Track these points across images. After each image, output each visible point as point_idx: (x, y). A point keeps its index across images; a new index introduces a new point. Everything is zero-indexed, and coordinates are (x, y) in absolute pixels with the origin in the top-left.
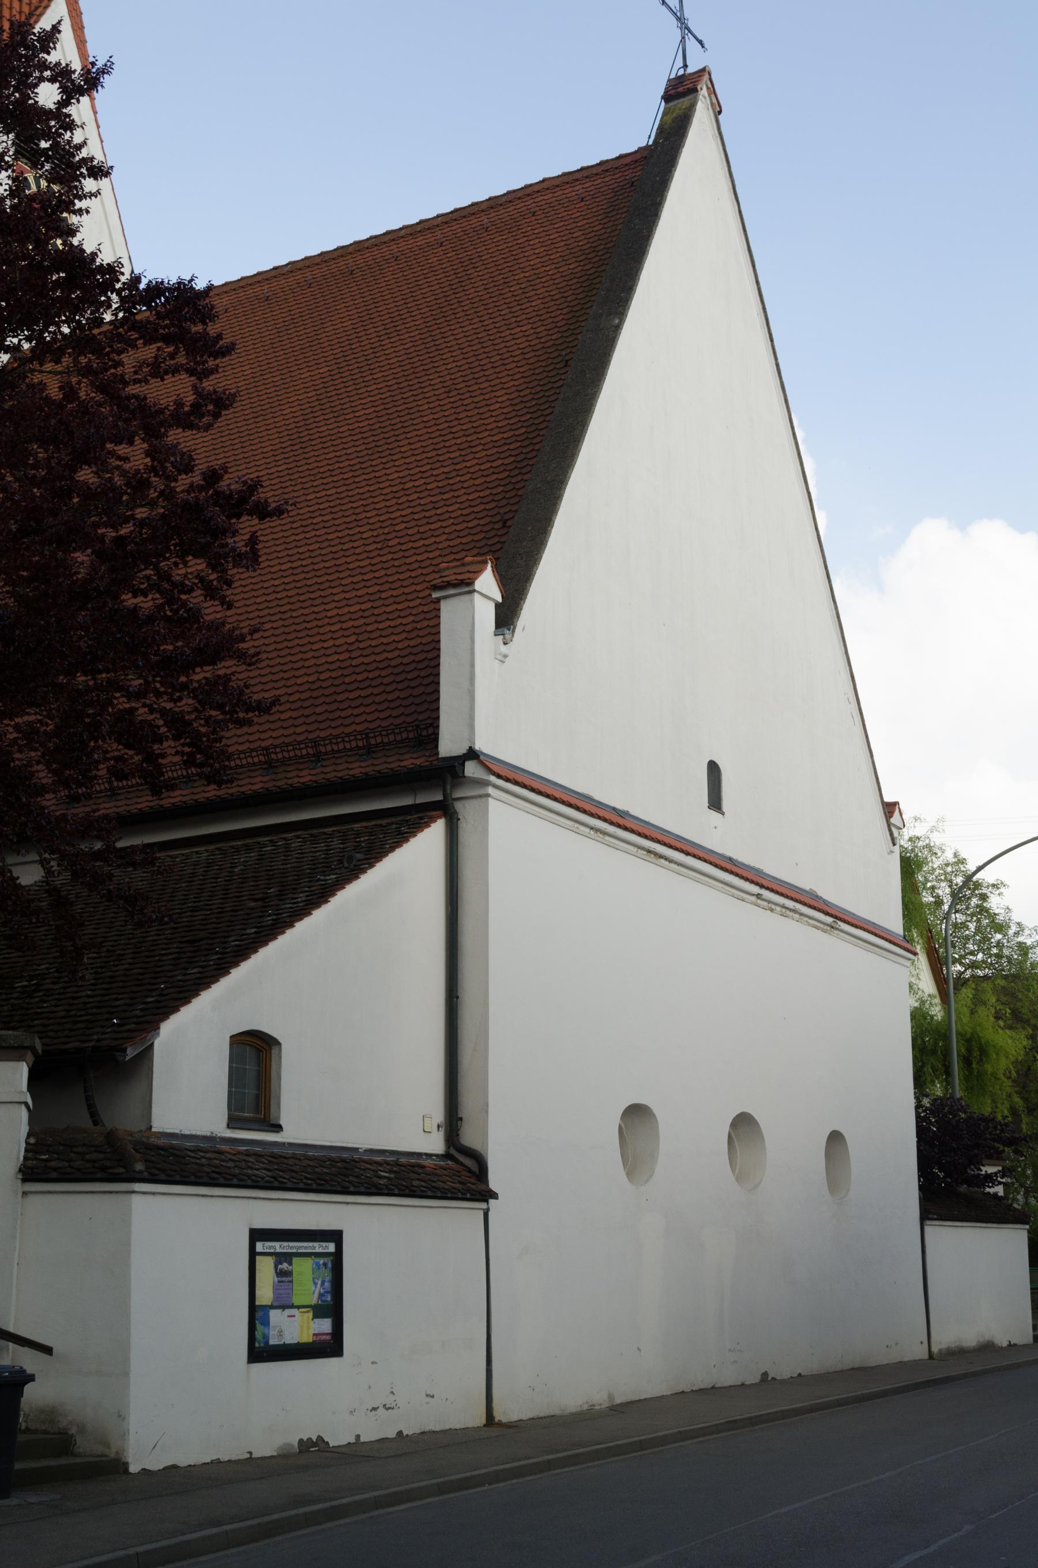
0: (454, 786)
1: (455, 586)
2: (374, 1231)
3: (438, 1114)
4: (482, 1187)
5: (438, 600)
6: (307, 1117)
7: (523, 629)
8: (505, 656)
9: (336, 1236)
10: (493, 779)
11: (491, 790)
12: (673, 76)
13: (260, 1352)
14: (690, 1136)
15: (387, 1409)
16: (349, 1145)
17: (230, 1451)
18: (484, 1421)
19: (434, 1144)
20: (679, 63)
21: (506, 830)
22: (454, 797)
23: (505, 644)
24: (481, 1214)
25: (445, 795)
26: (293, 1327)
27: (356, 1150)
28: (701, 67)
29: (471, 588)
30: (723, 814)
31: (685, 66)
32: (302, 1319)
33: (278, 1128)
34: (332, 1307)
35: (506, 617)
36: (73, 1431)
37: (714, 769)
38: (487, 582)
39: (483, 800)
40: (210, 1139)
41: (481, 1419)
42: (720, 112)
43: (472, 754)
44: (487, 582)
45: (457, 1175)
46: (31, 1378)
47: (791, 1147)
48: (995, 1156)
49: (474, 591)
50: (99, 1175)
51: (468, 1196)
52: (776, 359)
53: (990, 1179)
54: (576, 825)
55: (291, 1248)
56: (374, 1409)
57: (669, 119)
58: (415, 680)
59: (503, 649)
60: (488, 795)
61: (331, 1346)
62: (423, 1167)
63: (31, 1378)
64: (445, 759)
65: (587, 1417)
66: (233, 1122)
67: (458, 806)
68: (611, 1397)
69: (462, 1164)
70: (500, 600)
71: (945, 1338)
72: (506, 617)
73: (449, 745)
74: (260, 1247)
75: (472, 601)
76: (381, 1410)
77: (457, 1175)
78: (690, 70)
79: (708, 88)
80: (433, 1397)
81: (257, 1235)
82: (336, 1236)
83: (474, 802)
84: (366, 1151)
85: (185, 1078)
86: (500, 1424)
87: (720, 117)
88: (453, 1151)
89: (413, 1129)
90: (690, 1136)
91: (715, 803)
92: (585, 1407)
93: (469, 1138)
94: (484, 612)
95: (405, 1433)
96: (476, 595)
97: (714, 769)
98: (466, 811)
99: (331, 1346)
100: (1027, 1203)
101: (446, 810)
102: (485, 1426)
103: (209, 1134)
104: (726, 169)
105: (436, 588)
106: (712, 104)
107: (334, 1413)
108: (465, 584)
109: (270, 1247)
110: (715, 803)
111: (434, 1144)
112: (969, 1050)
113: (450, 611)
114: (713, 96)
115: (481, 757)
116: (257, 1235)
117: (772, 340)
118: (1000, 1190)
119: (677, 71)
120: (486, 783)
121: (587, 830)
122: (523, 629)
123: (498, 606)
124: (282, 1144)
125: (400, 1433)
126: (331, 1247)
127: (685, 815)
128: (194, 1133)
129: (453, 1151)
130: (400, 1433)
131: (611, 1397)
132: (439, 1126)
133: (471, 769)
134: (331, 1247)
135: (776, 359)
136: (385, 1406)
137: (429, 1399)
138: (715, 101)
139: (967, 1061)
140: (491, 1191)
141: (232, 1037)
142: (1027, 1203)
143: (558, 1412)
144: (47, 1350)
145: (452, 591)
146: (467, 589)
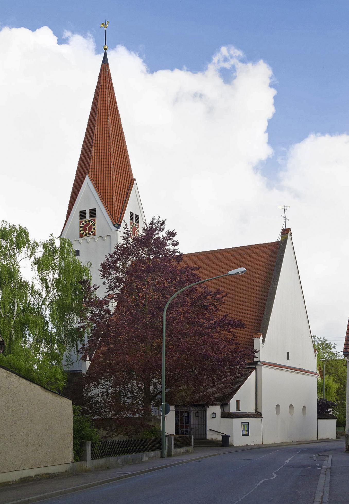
2: (252, 421)
6: (243, 410)
9: (248, 423)
14: (284, 408)
16: (32, 473)
17: (241, 445)
21: (265, 371)
26: (245, 433)
32: (246, 432)
34: (248, 431)
35: (263, 341)
37: (288, 353)
38: (261, 337)
43: (259, 361)
45: (258, 415)
47: (298, 409)
48: (331, 408)
53: (330, 411)
58: (252, 352)
61: (248, 435)
65: (272, 444)
71: (320, 437)
72: (263, 341)
77: (258, 415)
81: (242, 423)
82: (248, 423)
84: (35, 476)
90: (284, 408)
94: (261, 341)
97: (288, 353)
100: (336, 414)
108: (258, 338)
111: (254, 411)
112: (327, 388)
113: (255, 341)
118: (331, 413)
139: (326, 390)
142: (336, 414)
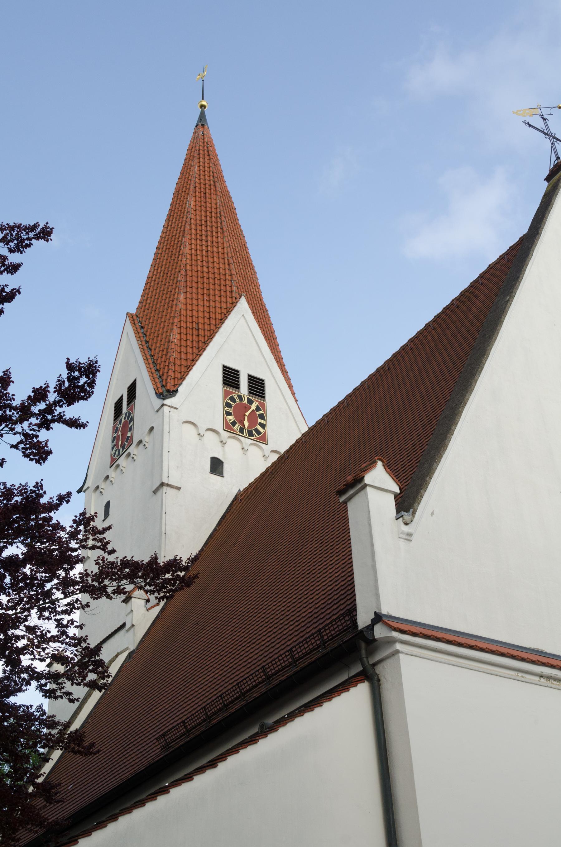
0: (371, 652)
5: (345, 503)
7: (432, 514)
8: (410, 535)
10: (395, 634)
11: (398, 646)
20: (554, 158)
21: (418, 678)
23: (406, 524)
25: (363, 665)
29: (362, 484)
30: (135, 380)
35: (406, 503)
38: (378, 477)
39: (396, 657)
43: (378, 618)
44: (378, 477)
49: (366, 485)
54: (520, 674)
57: (550, 188)
59: (405, 529)
60: (397, 652)
72: (406, 503)
73: (363, 619)
75: (366, 494)
83: (389, 662)
96: (368, 488)
98: (385, 671)
101: (370, 676)
105: (341, 493)
108: (356, 483)
115: (384, 619)
120: (392, 641)
121: (537, 678)
122: (432, 514)
123: (396, 496)
133: (380, 632)
145: (351, 492)
146: (360, 486)
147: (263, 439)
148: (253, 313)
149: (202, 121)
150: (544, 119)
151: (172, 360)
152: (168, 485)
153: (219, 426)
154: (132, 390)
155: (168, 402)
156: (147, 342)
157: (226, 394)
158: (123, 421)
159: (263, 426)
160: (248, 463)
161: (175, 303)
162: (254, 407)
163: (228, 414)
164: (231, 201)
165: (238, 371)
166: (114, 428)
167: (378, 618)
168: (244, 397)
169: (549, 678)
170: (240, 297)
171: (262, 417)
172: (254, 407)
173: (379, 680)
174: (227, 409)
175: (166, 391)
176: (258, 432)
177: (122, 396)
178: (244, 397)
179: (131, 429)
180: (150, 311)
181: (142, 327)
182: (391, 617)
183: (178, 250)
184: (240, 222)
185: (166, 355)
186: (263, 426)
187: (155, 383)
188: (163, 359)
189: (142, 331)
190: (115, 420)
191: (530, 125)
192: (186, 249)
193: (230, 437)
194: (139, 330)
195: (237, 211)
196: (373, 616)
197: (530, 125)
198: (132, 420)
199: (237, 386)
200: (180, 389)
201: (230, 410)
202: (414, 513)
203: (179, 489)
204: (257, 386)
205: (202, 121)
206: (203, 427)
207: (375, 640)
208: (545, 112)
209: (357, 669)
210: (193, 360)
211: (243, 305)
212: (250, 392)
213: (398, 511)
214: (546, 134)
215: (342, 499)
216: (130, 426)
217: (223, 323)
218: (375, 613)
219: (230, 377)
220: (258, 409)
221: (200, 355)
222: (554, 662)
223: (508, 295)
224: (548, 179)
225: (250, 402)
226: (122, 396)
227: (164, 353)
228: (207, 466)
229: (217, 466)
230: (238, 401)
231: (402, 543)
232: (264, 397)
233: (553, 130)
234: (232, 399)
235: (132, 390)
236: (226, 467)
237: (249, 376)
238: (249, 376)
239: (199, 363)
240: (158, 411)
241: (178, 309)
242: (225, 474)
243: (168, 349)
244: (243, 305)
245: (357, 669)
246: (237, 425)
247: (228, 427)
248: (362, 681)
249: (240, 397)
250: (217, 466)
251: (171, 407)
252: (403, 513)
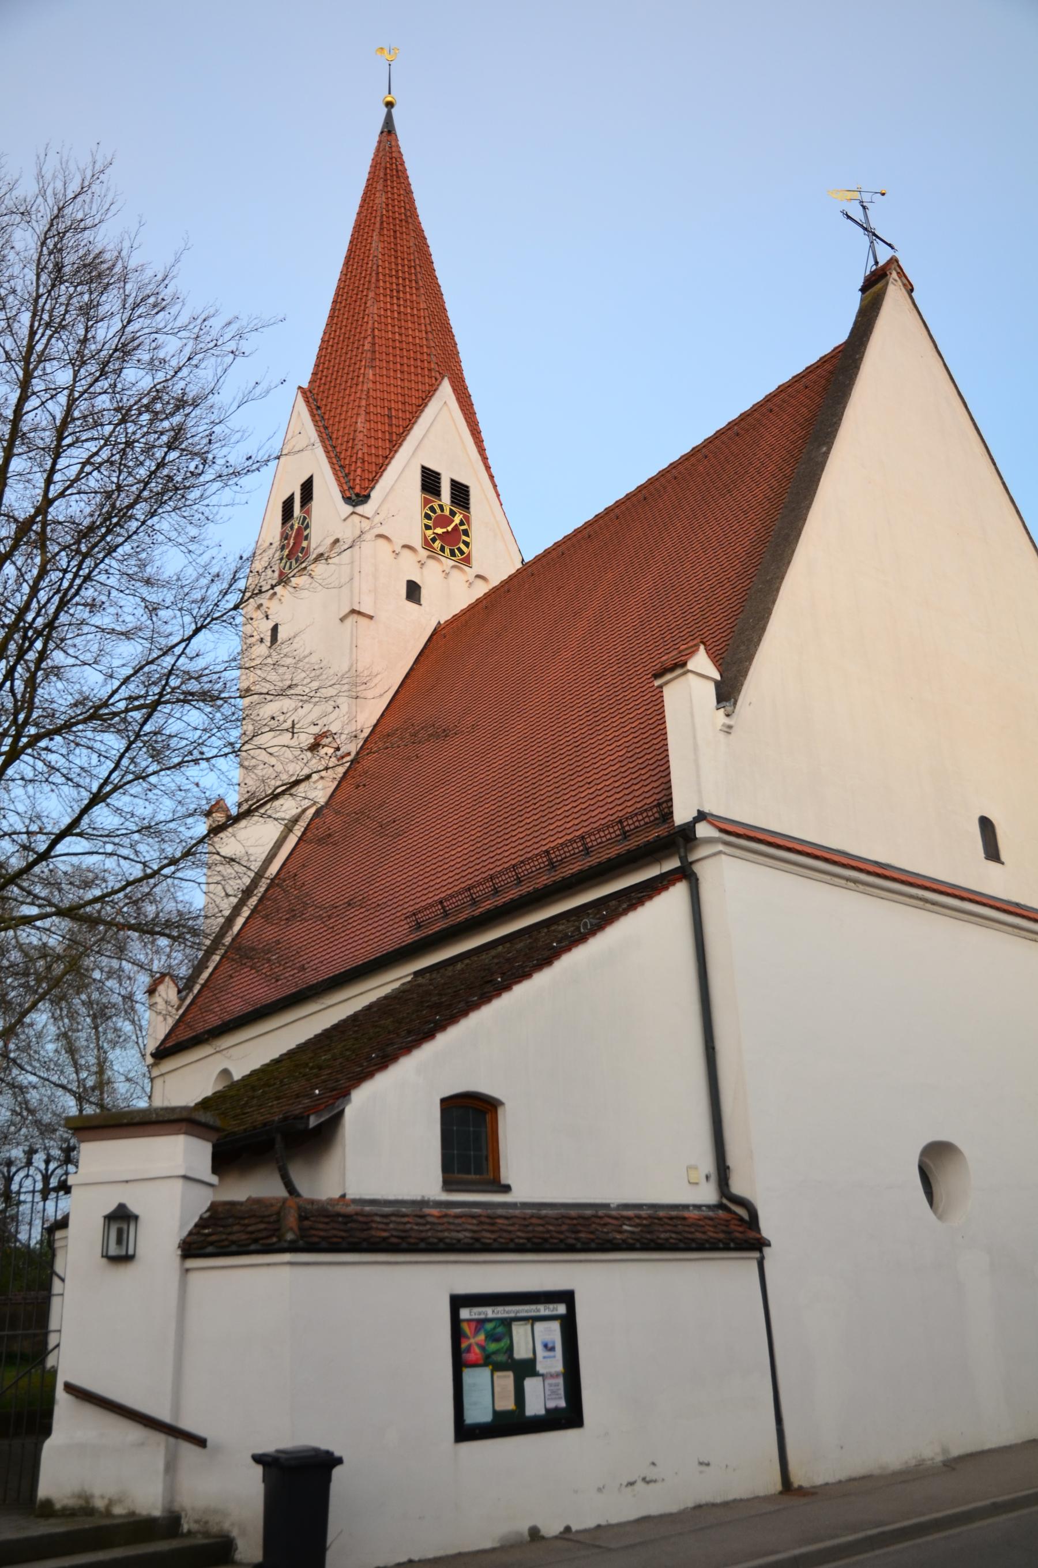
1: (672, 669)
3: (707, 1164)
4: (752, 1234)
5: (661, 687)
6: (534, 1172)
8: (730, 727)
9: (567, 1297)
12: (868, 273)
13: (465, 1432)
15: (648, 1482)
18: (779, 1487)
19: (707, 1194)
20: (872, 262)
22: (690, 860)
23: (728, 715)
24: (754, 1265)
27: (606, 1206)
28: (888, 258)
29: (685, 669)
30: (312, 477)
31: (877, 263)
33: (507, 1189)
35: (727, 692)
36: (235, 1533)
37: (986, 825)
38: (701, 662)
40: (423, 1203)
41: (775, 1484)
42: (912, 290)
44: (701, 662)
46: (339, 1461)
50: (253, 1247)
51: (721, 1245)
52: (1001, 478)
55: (508, 1312)
56: (631, 1484)
57: (866, 302)
62: (684, 1218)
63: (339, 1461)
64: (679, 826)
66: (448, 1185)
67: (697, 868)
68: (945, 1451)
69: (735, 1213)
70: (718, 677)
72: (727, 692)
73: (682, 815)
74: (465, 1313)
76: (640, 1485)
78: (881, 264)
79: (898, 273)
80: (708, 1464)
81: (458, 1302)
82: (567, 1297)
85: (385, 1141)
86: (801, 1492)
87: (913, 294)
88: (725, 1201)
89: (679, 1181)
91: (992, 853)
92: (913, 1463)
93: (738, 1187)
95: (574, 1528)
97: (986, 825)
99: (569, 1416)
101: (686, 874)
102: (781, 1493)
103: (419, 1198)
104: (926, 333)
105: (657, 676)
106: (904, 285)
107: (576, 1492)
109: (480, 1314)
110: (992, 853)
111: (707, 1194)
114: (903, 279)
115: (709, 818)
116: (458, 1302)
117: (994, 464)
119: (871, 267)
123: (718, 685)
124: (514, 1205)
125: (568, 1529)
126: (561, 1309)
127: (964, 866)
128: (400, 1198)
129: (725, 1201)
130: (568, 1529)
131: (945, 1451)
132: (707, 1177)
133: (703, 830)
134: (561, 1309)
135: (1001, 478)
136: (644, 1479)
137: (703, 1468)
138: (905, 281)
140: (762, 1238)
141: (443, 1101)
143: (877, 1472)
144: (201, 1442)
145: (668, 677)
147: (467, 560)
148: (458, 399)
149: (388, 129)
150: (864, 208)
151: (360, 455)
152: (359, 613)
153: (417, 542)
154: (307, 488)
155: (360, 509)
156: (326, 428)
157: (426, 502)
158: (296, 527)
159: (467, 544)
160: (451, 593)
161: (361, 379)
162: (457, 520)
163: (428, 527)
164: (426, 244)
165: (439, 474)
166: (282, 534)
167: (701, 816)
168: (449, 508)
169: (855, 881)
170: (443, 379)
171: (466, 533)
172: (457, 520)
173: (697, 880)
174: (426, 521)
175: (356, 497)
176: (462, 552)
177: (293, 494)
178: (449, 508)
179: (306, 538)
180: (327, 387)
181: (319, 408)
182: (712, 815)
183: (362, 308)
184: (438, 274)
185: (353, 448)
186: (467, 544)
187: (340, 485)
188: (349, 453)
189: (319, 412)
190: (283, 524)
191: (849, 217)
192: (373, 309)
193: (429, 557)
194: (315, 412)
195: (434, 258)
196: (695, 814)
197: (849, 217)
198: (307, 527)
199: (437, 493)
200: (373, 494)
201: (430, 523)
202: (735, 704)
203: (371, 617)
204: (461, 494)
205: (388, 129)
206: (398, 542)
207: (696, 838)
208: (866, 197)
209: (673, 864)
210: (386, 457)
211: (446, 389)
212: (452, 502)
213: (718, 702)
214: (865, 229)
215: (657, 683)
216: (305, 533)
217: (422, 411)
218: (699, 811)
219: (430, 481)
220: (462, 523)
221: (396, 451)
222: (1032, 915)
223: (824, 444)
224: (863, 290)
225: (453, 513)
226: (293, 494)
227: (350, 444)
228: (403, 591)
229: (413, 591)
230: (438, 511)
231: (722, 735)
232: (468, 508)
233: (873, 224)
234: (432, 509)
235: (307, 488)
236: (424, 592)
237: (423, 467)
238: (423, 467)
239: (394, 462)
240: (345, 520)
241: (365, 388)
242: (422, 601)
243: (354, 440)
244: (446, 389)
245: (673, 864)
246: (438, 542)
247: (427, 544)
248: (679, 880)
249: (441, 507)
250: (413, 591)
251: (362, 516)
252: (724, 704)
